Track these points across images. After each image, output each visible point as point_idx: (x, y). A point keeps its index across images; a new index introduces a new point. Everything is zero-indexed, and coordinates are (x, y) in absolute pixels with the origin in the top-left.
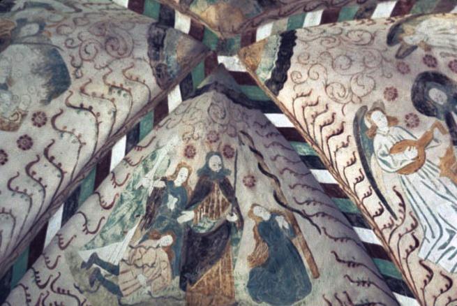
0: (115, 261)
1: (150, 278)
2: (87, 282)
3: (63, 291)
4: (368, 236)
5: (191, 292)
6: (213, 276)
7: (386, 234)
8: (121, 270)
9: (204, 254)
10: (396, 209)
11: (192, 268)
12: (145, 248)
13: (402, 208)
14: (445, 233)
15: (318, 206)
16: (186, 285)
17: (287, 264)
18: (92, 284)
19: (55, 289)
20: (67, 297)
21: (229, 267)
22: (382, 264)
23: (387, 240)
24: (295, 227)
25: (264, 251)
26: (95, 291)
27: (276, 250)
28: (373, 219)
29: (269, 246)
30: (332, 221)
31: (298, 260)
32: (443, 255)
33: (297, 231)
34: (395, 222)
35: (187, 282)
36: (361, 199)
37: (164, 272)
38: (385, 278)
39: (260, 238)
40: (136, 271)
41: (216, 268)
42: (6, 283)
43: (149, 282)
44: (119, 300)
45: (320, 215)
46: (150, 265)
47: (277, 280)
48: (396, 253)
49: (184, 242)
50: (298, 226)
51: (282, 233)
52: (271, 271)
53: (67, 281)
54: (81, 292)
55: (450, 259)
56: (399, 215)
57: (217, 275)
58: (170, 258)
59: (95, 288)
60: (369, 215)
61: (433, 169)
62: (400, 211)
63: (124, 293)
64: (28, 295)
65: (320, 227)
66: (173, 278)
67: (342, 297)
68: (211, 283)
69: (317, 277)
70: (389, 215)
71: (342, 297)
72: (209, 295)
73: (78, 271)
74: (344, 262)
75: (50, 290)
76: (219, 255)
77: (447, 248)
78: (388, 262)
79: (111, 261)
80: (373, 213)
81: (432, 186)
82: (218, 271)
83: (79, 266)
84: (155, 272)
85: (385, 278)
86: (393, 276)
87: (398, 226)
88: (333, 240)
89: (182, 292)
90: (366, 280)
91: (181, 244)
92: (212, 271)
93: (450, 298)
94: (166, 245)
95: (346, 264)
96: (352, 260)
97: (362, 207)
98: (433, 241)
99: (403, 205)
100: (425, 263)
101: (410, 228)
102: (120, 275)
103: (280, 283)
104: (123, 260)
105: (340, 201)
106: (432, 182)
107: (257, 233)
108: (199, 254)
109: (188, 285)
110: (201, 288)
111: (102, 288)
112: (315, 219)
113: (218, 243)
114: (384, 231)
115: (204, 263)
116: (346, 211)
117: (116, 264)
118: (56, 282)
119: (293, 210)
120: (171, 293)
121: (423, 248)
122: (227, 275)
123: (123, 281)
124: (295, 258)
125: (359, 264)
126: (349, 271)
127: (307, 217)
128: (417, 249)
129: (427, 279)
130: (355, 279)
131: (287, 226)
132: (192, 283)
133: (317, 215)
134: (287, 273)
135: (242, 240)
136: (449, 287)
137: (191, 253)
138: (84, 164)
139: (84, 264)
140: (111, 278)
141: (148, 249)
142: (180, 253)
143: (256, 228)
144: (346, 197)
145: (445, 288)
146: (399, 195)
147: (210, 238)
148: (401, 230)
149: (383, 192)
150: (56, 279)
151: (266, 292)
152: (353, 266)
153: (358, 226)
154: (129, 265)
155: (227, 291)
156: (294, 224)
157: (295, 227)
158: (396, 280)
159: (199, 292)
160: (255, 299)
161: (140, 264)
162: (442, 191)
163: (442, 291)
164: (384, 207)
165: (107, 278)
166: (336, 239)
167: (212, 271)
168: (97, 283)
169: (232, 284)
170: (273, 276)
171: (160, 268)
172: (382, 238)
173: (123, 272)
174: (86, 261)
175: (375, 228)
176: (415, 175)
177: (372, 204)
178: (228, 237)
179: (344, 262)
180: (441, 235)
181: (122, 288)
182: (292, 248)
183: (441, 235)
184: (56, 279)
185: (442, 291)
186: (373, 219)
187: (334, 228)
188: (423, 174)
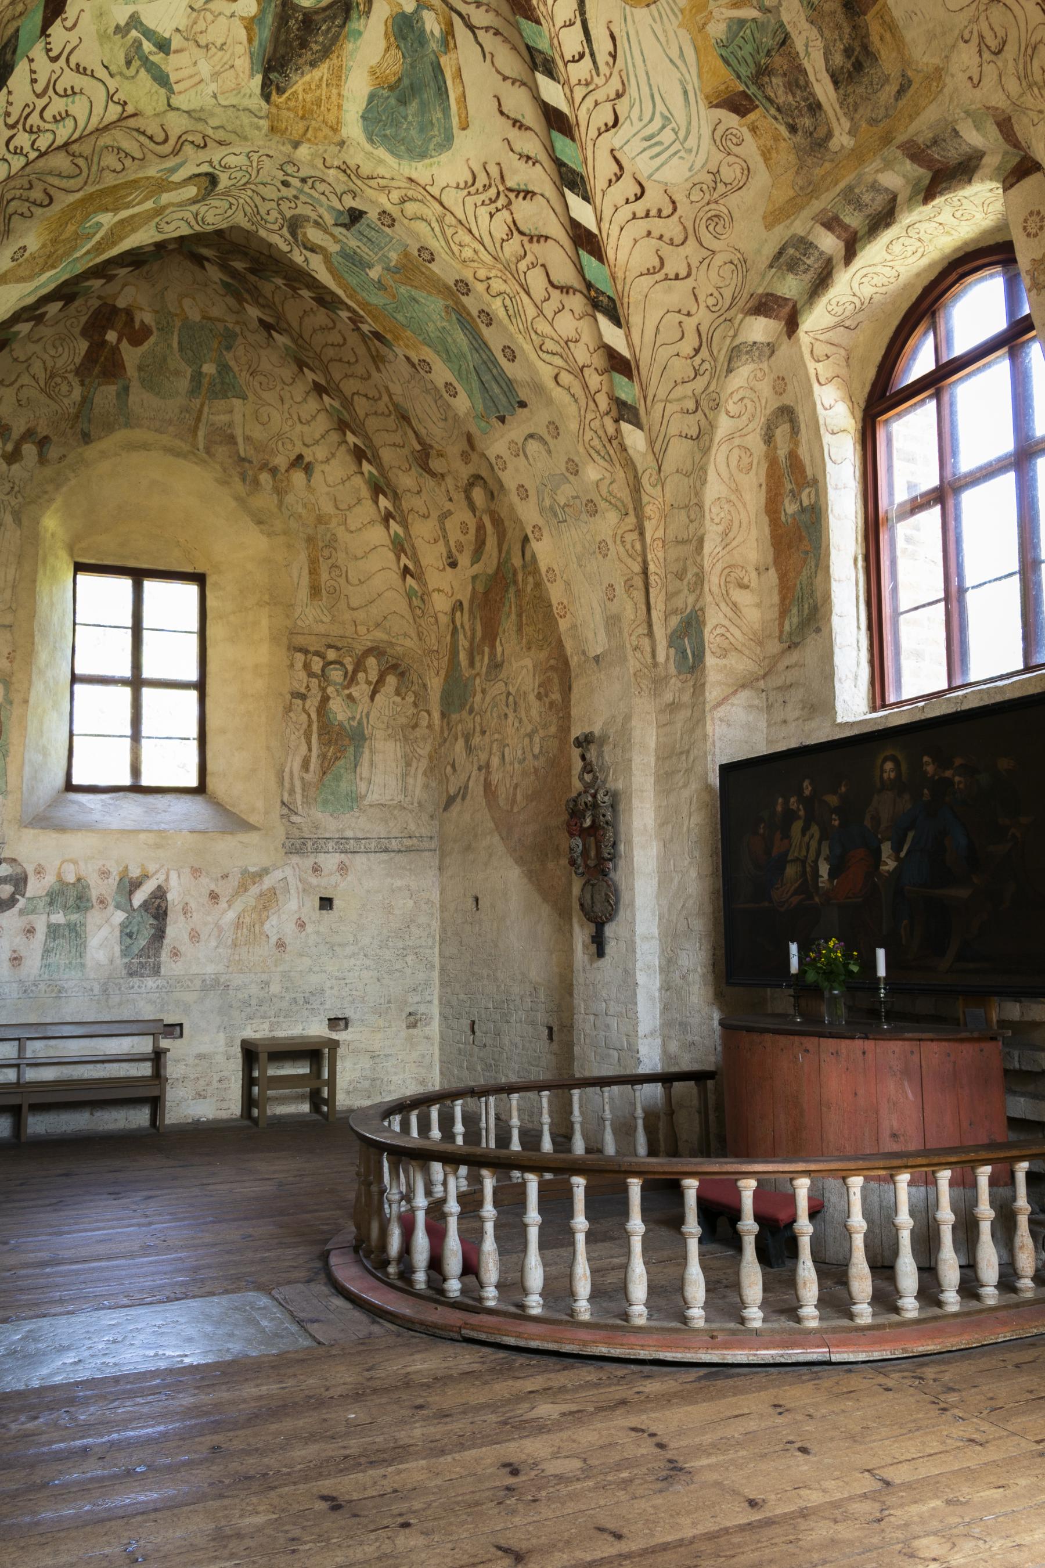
0: (165, 30)
1: (217, 68)
2: (122, 61)
3: (85, 69)
4: (552, 93)
5: (277, 106)
6: (313, 87)
7: (579, 92)
8: (173, 47)
9: (304, 45)
10: (602, 57)
11: (282, 66)
12: (212, 12)
13: (611, 61)
14: (658, 115)
15: (491, 15)
16: (270, 93)
17: (425, 96)
18: (129, 63)
19: (73, 65)
20: (90, 79)
21: (338, 77)
22: (560, 141)
23: (577, 105)
24: (450, 38)
25: (395, 65)
26: (133, 77)
27: (413, 66)
28: (566, 65)
29: (404, 56)
30: (508, 46)
31: (442, 92)
32: (645, 150)
33: (452, 45)
34: (596, 80)
35: (273, 87)
36: (557, 27)
37: (238, 63)
38: (559, 164)
39: (392, 39)
40: (195, 50)
41: (320, 74)
42: (8, 57)
43: (215, 76)
44: (168, 99)
45: (492, 31)
46: (218, 45)
47: (405, 118)
48: (583, 129)
49: (276, 15)
50: (453, 37)
51: (427, 42)
52: (399, 100)
53: (90, 55)
54: (112, 76)
55: (652, 158)
56: (604, 69)
57: (319, 86)
58: (250, 40)
59: (132, 71)
60: (562, 56)
61: (672, 10)
62: (607, 63)
63: (176, 88)
64: (33, 72)
65: (487, 50)
66: (252, 76)
67: (494, 171)
68: (309, 97)
69: (464, 129)
70: (591, 65)
71: (494, 171)
72: (303, 118)
73: (109, 38)
74: (508, 117)
75: (65, 66)
76: (326, 52)
77: (653, 141)
78: (568, 141)
79: (160, 30)
80: (568, 57)
81: (663, 39)
82: (321, 79)
83: (111, 31)
84: (225, 60)
85: (559, 164)
86: (570, 164)
87: (597, 87)
88: (500, 78)
89: (264, 104)
90: (531, 154)
91: (269, 19)
92: (312, 78)
93: (634, 214)
94: (245, 15)
95: (511, 122)
96: (520, 118)
97: (555, 41)
98: (638, 125)
99: (614, 56)
100: (618, 154)
101: (613, 96)
102: (172, 56)
103: (410, 123)
104: (177, 30)
105: (526, 25)
106: (665, 31)
107: (390, 30)
108: (296, 43)
109: (274, 93)
110: (292, 104)
111: (143, 72)
112: (480, 33)
113: (329, 29)
114: (577, 89)
115: (301, 61)
116: (531, 44)
117: (167, 35)
118: (76, 51)
119: (452, 9)
120: (247, 102)
121: (621, 132)
122: (334, 91)
123: (173, 65)
124: (439, 89)
125: (528, 128)
126: (513, 134)
127: (471, 28)
128: (613, 131)
129: (614, 179)
130: (517, 148)
131: (437, 33)
132: (281, 91)
133: (487, 29)
134: (424, 107)
135: (366, 36)
136: (638, 198)
137: (283, 38)
138: (622, 806)
139: (118, 29)
140: (157, 58)
141: (216, 17)
142: (267, 33)
143: (390, 21)
144: (538, 22)
145: (632, 198)
146: (613, 38)
147: (315, 17)
148: (600, 95)
149: (590, 26)
150: (75, 48)
151: (388, 132)
152: (520, 128)
153: (543, 73)
154: (187, 39)
155: (331, 118)
156: (449, 32)
157: (450, 38)
158: (573, 172)
159: (289, 109)
160: (371, 140)
161: (203, 41)
162: (674, 54)
163: (627, 202)
164: (587, 51)
165: (151, 58)
166: (505, 78)
167: (312, 78)
168: (136, 63)
169: (340, 107)
170: (402, 109)
171: (233, 54)
172: (571, 101)
173: (177, 51)
174: (122, 23)
175: (565, 83)
176: (645, 11)
177: (571, 41)
178: (344, 23)
179: (508, 117)
180: (651, 120)
181: (172, 79)
182: (438, 69)
183: (651, 120)
184: (75, 48)
185: (627, 202)
186: (566, 65)
187: (509, 62)
188: (656, 15)
